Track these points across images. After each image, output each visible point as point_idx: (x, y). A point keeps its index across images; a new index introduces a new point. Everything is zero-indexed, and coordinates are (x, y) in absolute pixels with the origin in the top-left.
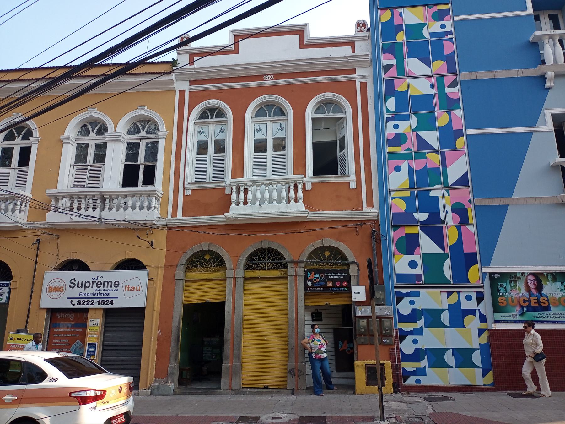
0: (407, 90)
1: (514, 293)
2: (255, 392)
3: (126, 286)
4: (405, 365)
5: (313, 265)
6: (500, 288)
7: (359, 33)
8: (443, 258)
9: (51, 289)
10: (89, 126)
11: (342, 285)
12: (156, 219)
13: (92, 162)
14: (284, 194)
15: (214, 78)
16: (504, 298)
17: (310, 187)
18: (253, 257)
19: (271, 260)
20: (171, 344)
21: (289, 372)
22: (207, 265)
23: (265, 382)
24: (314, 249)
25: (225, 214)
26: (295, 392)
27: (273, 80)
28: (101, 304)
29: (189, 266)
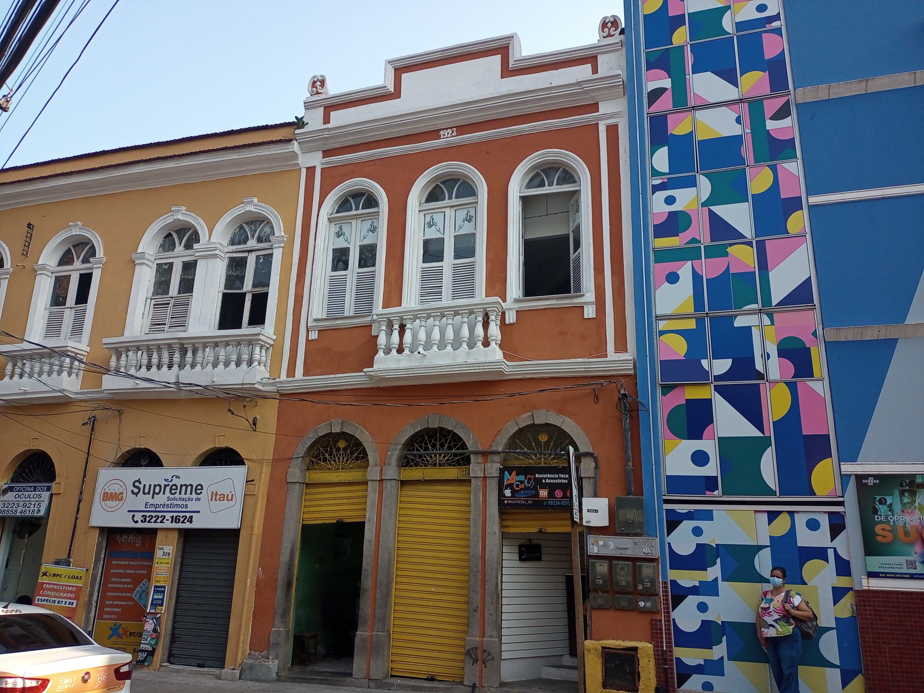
0: (692, 131)
1: (909, 518)
3: (213, 492)
5: (517, 459)
6: (878, 506)
8: (759, 445)
9: (107, 497)
10: (175, 236)
12: (260, 380)
14: (465, 332)
16: (887, 527)
17: (513, 318)
19: (446, 450)
20: (276, 592)
21: (468, 653)
22: (341, 458)
23: (430, 669)
24: (517, 429)
27: (454, 136)
28: (176, 522)
29: (313, 459)
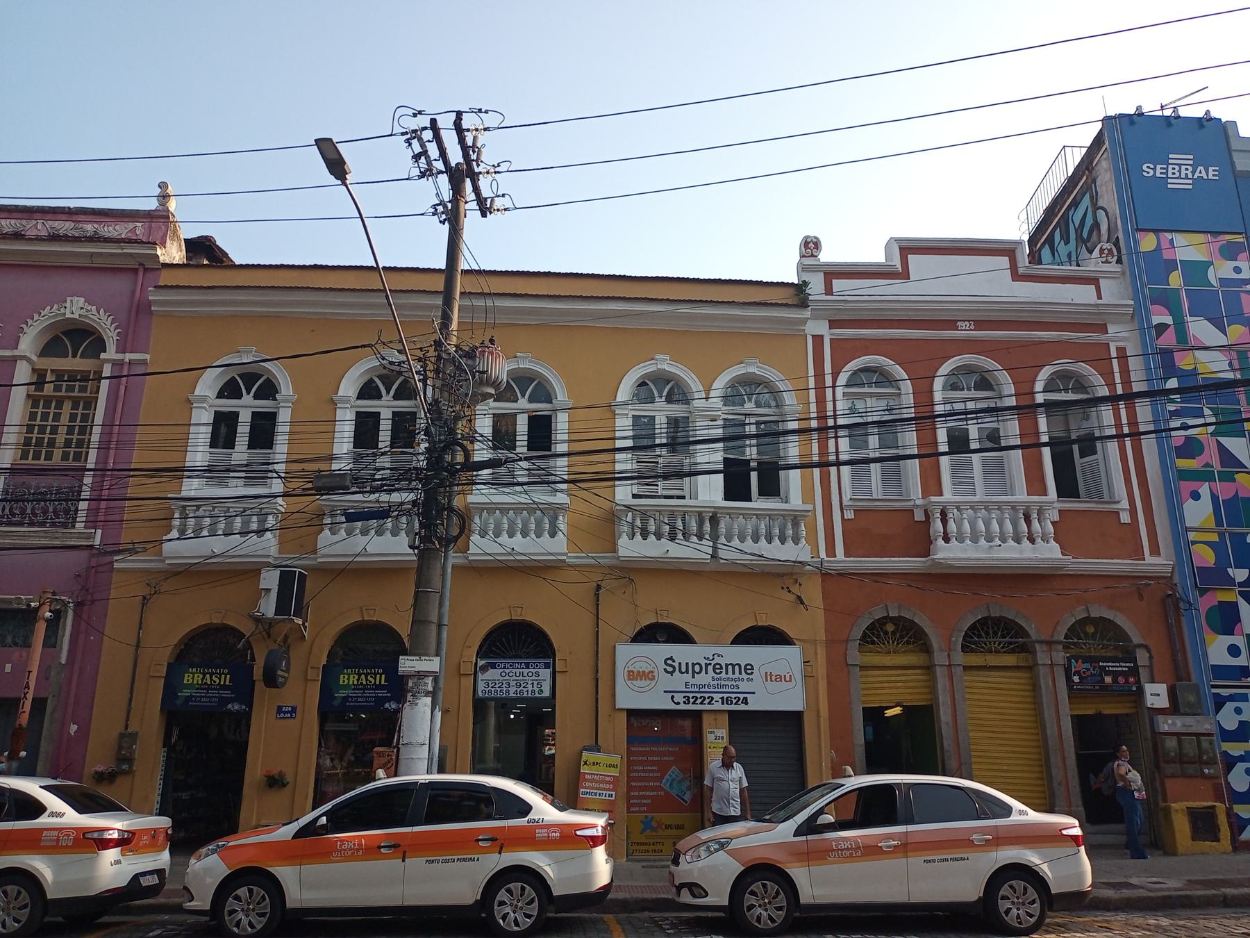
3: (766, 673)
7: (1104, 264)
9: (632, 675)
11: (1127, 682)
28: (728, 704)
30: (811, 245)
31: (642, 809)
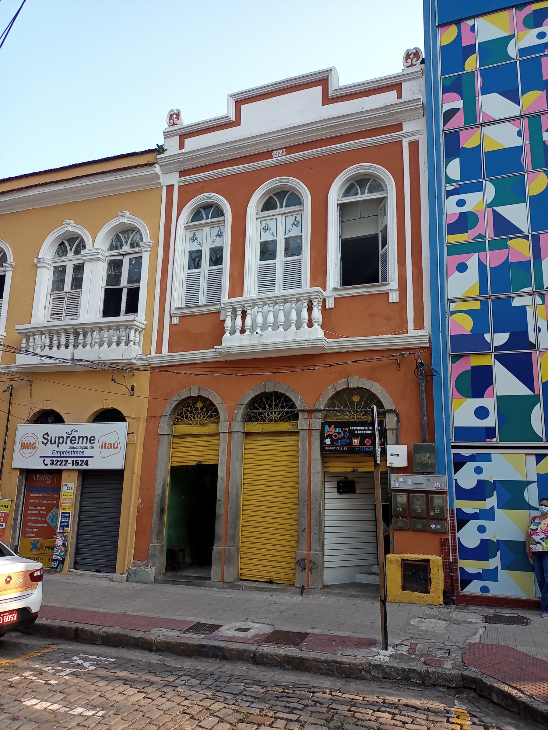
2: (254, 588)
3: (103, 442)
4: (464, 564)
7: (408, 68)
8: (531, 401)
10: (67, 244)
13: (70, 289)
15: (209, 163)
18: (256, 405)
19: (280, 409)
21: (298, 563)
23: (269, 575)
25: (215, 347)
26: (305, 591)
28: (76, 465)
29: (178, 417)
30: (175, 116)
31: (32, 535)
